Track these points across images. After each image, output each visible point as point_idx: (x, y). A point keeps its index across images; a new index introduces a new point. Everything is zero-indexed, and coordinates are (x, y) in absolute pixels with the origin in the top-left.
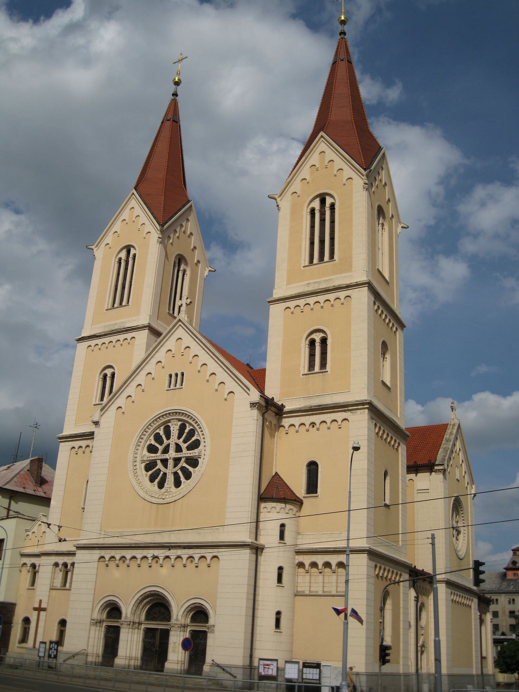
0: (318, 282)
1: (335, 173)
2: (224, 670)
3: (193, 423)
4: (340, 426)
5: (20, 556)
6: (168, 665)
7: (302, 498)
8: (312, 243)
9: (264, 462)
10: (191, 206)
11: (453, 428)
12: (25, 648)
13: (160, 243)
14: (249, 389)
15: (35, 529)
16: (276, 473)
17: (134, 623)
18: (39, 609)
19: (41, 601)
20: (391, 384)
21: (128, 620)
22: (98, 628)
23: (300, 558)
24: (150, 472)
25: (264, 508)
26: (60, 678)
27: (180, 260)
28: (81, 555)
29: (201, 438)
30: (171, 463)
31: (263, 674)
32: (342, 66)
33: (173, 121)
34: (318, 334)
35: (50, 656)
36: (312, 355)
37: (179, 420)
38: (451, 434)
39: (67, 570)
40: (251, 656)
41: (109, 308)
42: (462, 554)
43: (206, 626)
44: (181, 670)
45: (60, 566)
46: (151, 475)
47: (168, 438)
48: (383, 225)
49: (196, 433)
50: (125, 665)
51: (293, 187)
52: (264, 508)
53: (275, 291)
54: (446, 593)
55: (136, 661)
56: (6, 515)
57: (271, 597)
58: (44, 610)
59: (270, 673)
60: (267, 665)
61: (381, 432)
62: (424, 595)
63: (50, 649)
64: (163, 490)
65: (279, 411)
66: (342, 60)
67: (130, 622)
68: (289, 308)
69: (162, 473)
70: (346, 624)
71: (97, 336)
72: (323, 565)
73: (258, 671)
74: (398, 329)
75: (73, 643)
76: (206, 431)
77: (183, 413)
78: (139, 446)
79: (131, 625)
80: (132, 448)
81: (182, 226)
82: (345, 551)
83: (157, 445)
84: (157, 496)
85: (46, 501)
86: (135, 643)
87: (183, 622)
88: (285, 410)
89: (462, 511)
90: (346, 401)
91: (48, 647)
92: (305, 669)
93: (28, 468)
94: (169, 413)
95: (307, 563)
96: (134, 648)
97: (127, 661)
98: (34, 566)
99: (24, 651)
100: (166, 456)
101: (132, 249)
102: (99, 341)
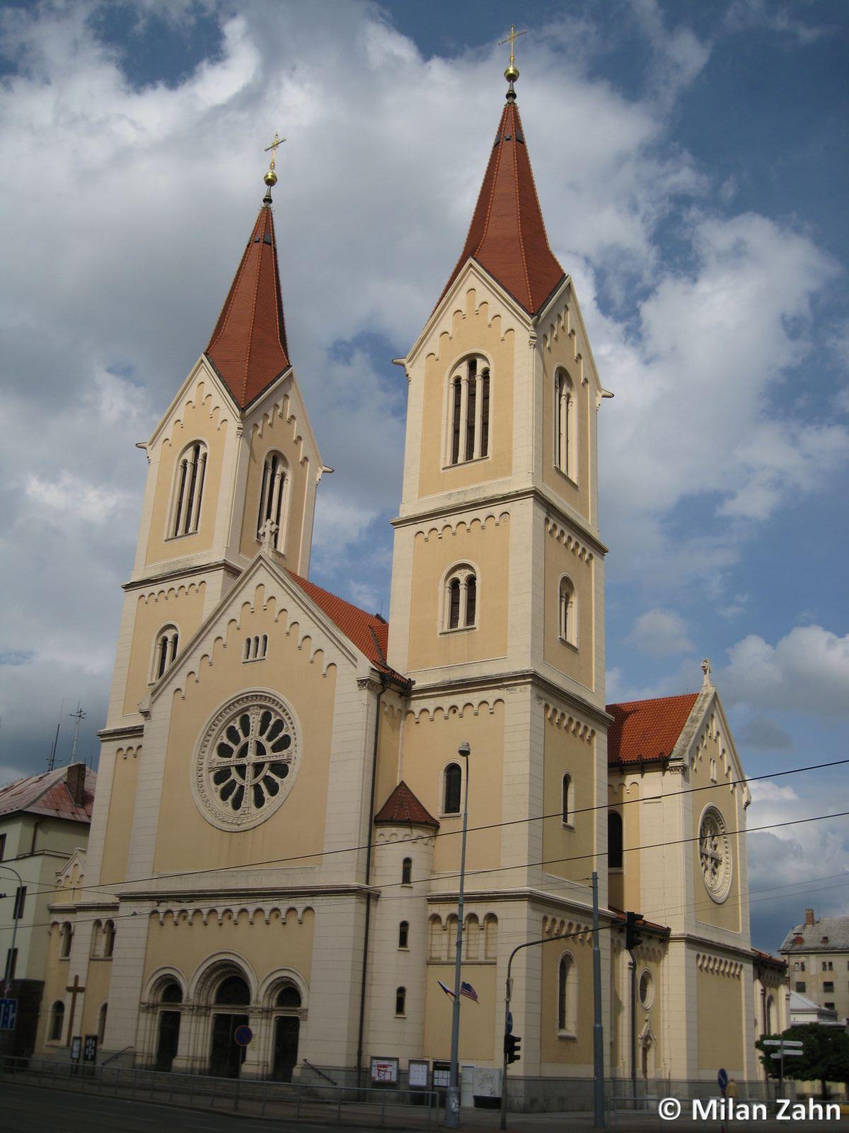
0: (462, 492)
1: (489, 321)
2: (320, 1073)
3: (280, 711)
4: (492, 711)
5: (48, 912)
7: (438, 819)
8: (456, 432)
9: (380, 767)
10: (291, 375)
11: (704, 701)
12: (56, 1047)
13: (241, 436)
14: (356, 660)
15: (69, 872)
16: (402, 783)
17: (199, 1007)
18: (75, 990)
19: (77, 978)
20: (580, 643)
21: (191, 1003)
22: (150, 1015)
23: (435, 909)
24: (222, 785)
25: (381, 835)
26: (242, 1104)
27: (276, 458)
28: (126, 908)
30: (250, 771)
31: (377, 1079)
32: (509, 147)
33: (265, 242)
34: (462, 571)
35: (86, 1057)
36: (455, 603)
37: (261, 707)
38: (700, 709)
40: (360, 1053)
41: (170, 537)
42: (722, 894)
43: (296, 1011)
44: (263, 1075)
45: (103, 926)
47: (246, 734)
48: (568, 396)
49: (285, 726)
50: (187, 1068)
51: (428, 345)
52: (381, 835)
53: (402, 508)
54: (687, 956)
55: (203, 1063)
56: (30, 851)
57: (391, 967)
58: (82, 990)
59: (387, 1077)
60: (384, 1066)
61: (558, 717)
62: (650, 960)
63: (87, 1047)
64: (239, 811)
65: (405, 689)
66: (508, 140)
67: (193, 1006)
68: (434, 529)
69: (237, 786)
70: (457, 1005)
71: (153, 581)
72: (485, 918)
73: (371, 1075)
74: (594, 555)
76: (298, 724)
77: (266, 697)
78: (206, 746)
79: (195, 1011)
80: (195, 750)
81: (276, 406)
82: (457, 899)
83: (231, 744)
85: (84, 827)
86: (201, 1036)
87: (265, 1005)
88: (415, 687)
89: (722, 828)
90: (501, 672)
91: (83, 1045)
92: (436, 1072)
93: (65, 779)
94: (247, 697)
95: (444, 916)
96: (200, 1043)
97: (190, 1062)
99: (53, 1051)
100: (244, 761)
101: (201, 446)
102: (155, 589)
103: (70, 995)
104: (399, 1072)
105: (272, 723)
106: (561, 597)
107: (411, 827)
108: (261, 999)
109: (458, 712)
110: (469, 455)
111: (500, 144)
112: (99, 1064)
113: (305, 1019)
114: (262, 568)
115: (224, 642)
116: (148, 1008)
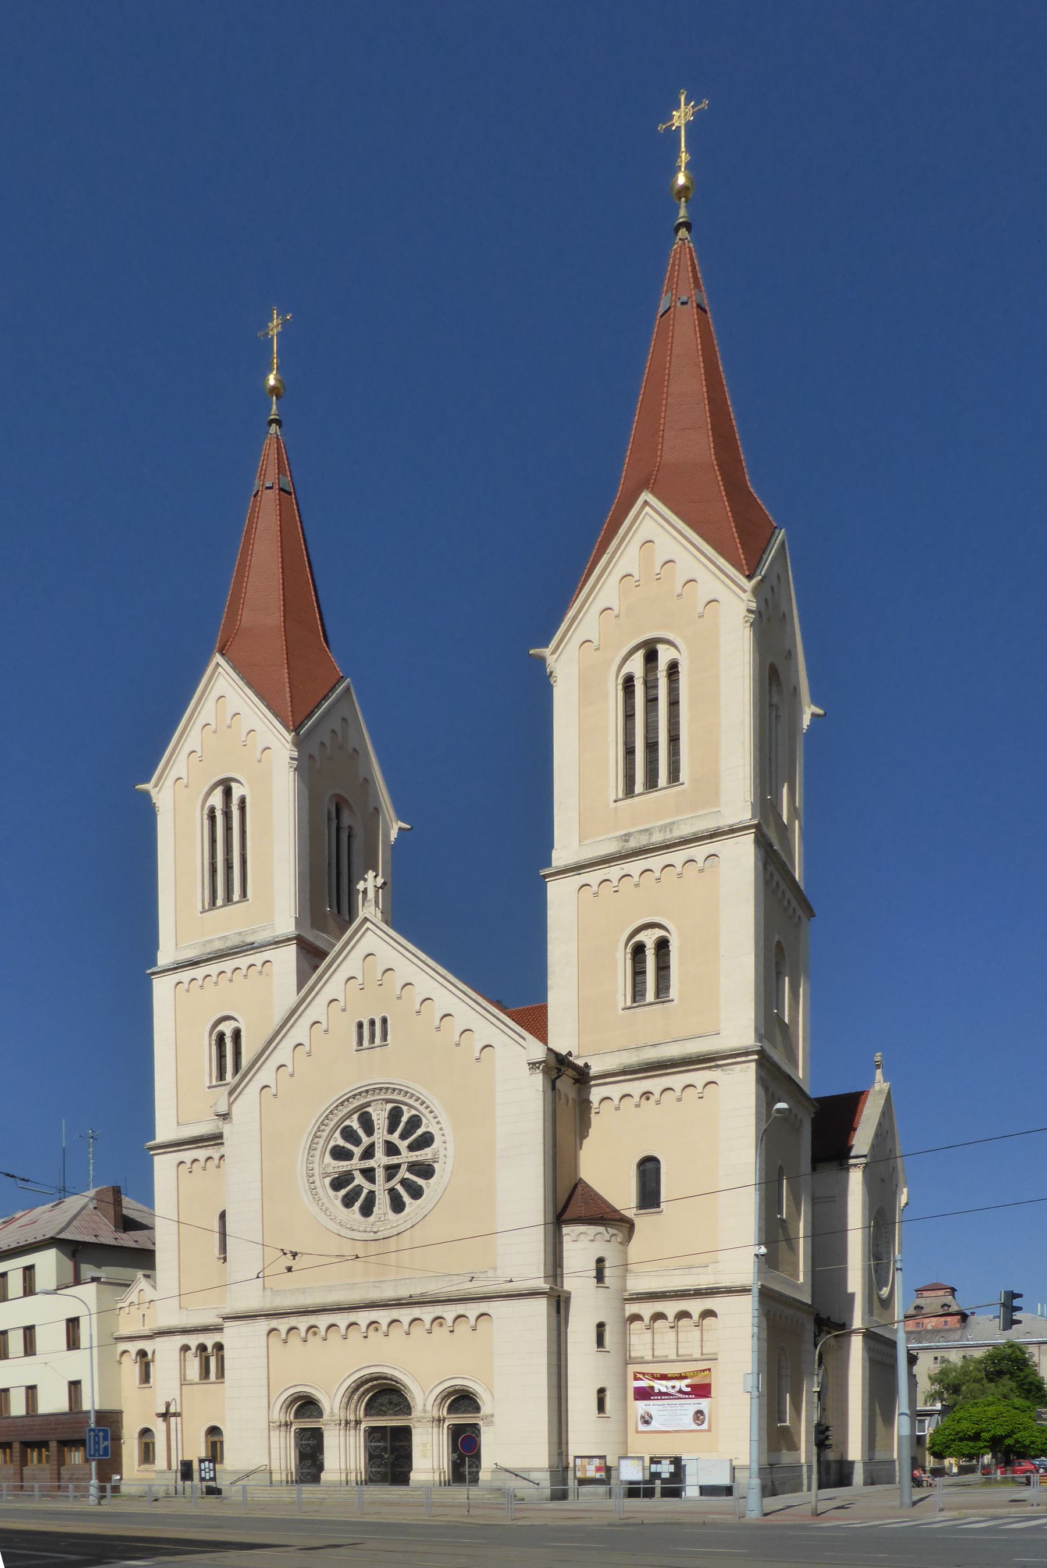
3: (417, 1104)
14: (524, 1039)
23: (631, 1309)
24: (343, 1192)
29: (433, 1129)
30: (380, 1174)
34: (649, 931)
37: (388, 1101)
75: (239, 1456)
84: (362, 1229)
98: (142, 1354)
99: (153, 1475)
101: (233, 785)
107: (604, 1225)
109: (653, 1099)
110: (228, 899)
111: (672, 309)
113: (491, 1423)
114: (369, 932)
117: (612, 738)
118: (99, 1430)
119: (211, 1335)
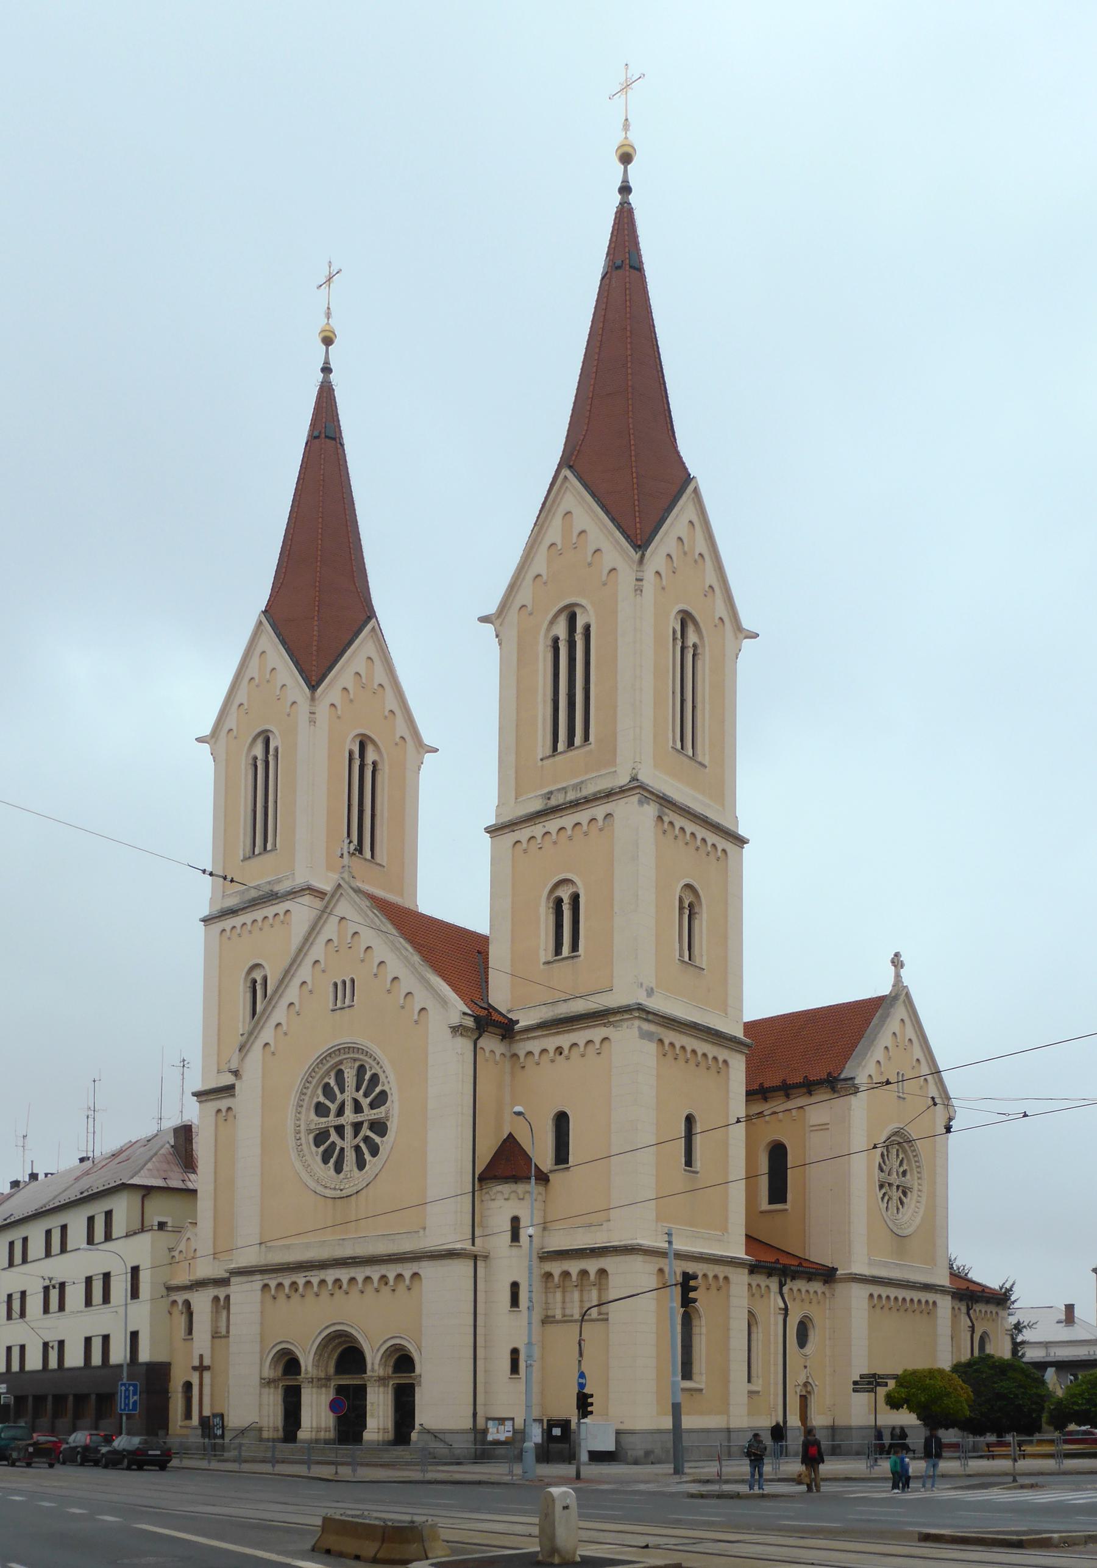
6: (367, 1436)
15: (182, 1246)
17: (319, 1379)
19: (201, 1356)
21: (309, 1376)
24: (322, 1148)
30: (349, 1131)
37: (355, 1060)
39: (222, 1305)
46: (325, 1152)
47: (342, 1091)
58: (208, 1368)
64: (342, 1175)
65: (507, 1030)
69: (338, 1148)
76: (392, 1078)
99: (184, 1431)
101: (578, 611)
103: (196, 1375)
104: (515, 1431)
105: (367, 1077)
106: (681, 908)
108: (376, 1367)
110: (571, 743)
112: (227, 1440)
115: (310, 987)
116: (268, 1383)
117: (540, 698)
118: (130, 1385)
119: (376, 1268)
